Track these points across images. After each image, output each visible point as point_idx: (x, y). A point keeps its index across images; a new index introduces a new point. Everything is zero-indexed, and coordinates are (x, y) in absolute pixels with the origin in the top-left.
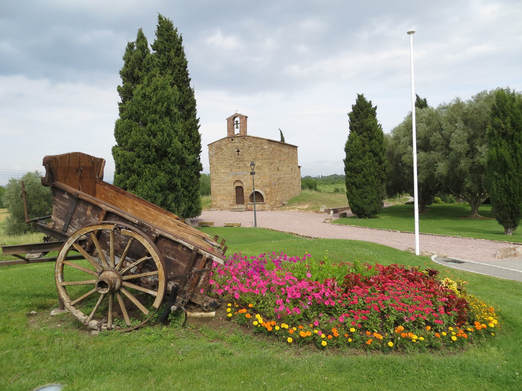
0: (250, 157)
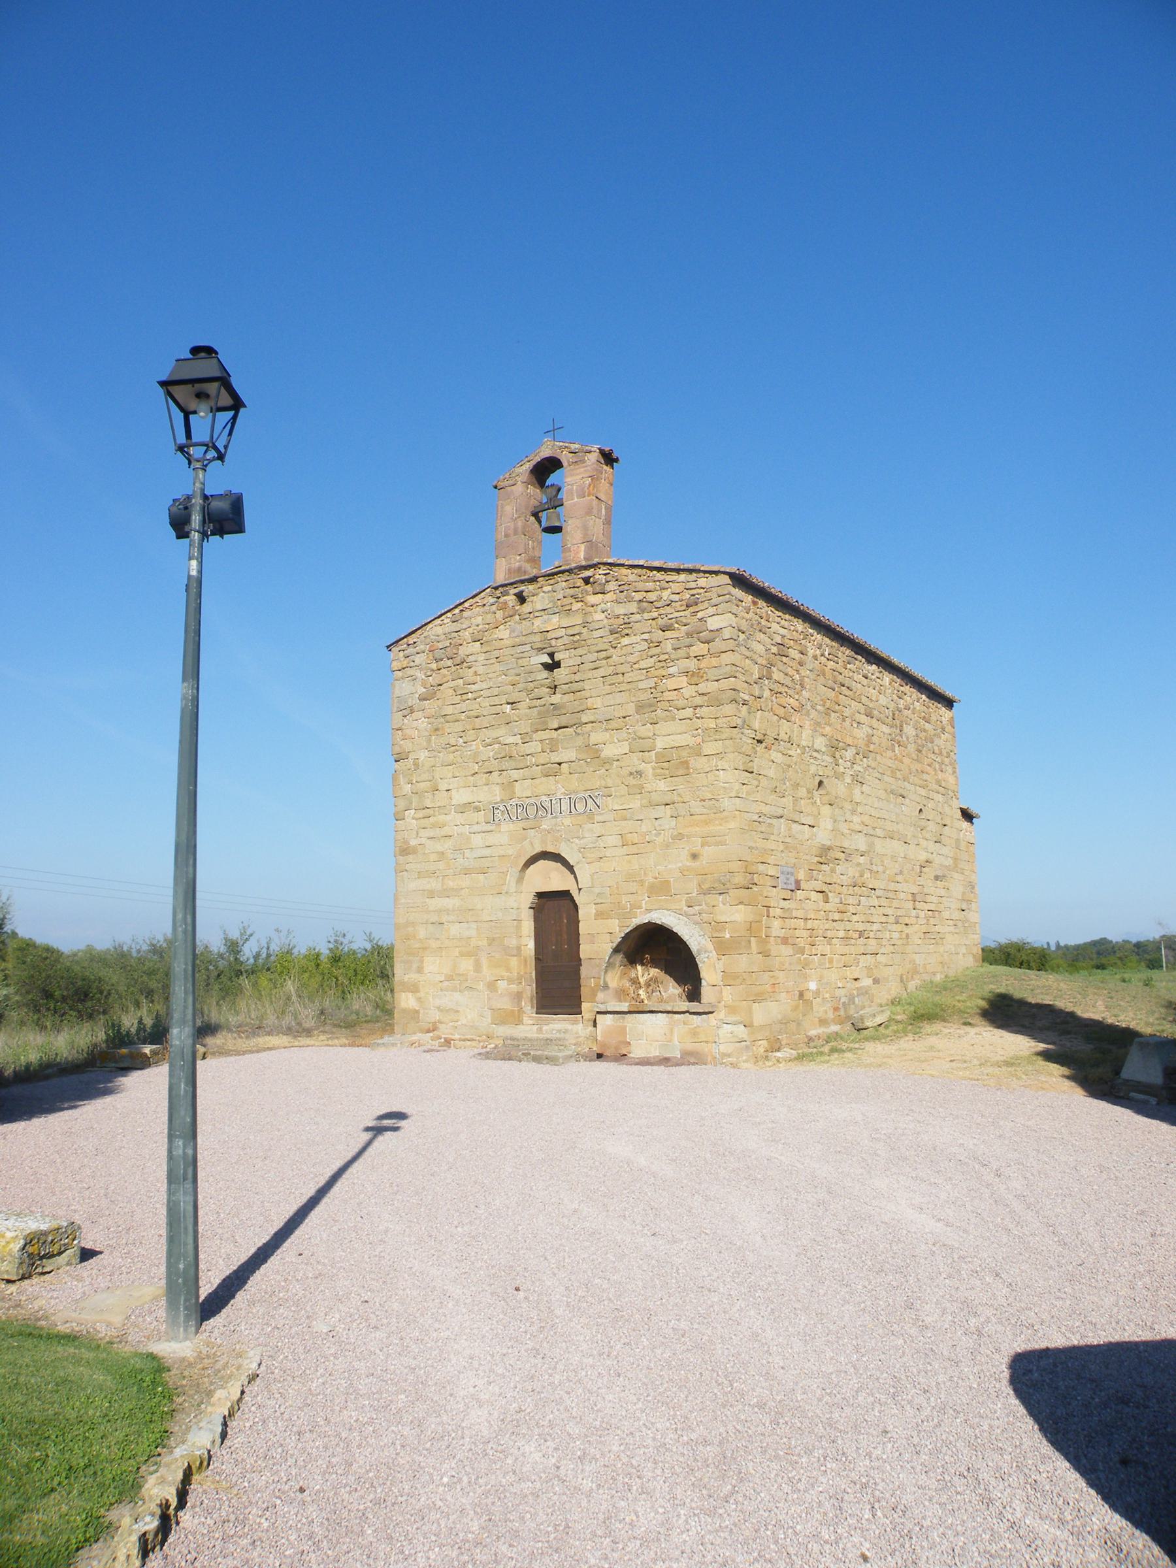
0: (619, 698)
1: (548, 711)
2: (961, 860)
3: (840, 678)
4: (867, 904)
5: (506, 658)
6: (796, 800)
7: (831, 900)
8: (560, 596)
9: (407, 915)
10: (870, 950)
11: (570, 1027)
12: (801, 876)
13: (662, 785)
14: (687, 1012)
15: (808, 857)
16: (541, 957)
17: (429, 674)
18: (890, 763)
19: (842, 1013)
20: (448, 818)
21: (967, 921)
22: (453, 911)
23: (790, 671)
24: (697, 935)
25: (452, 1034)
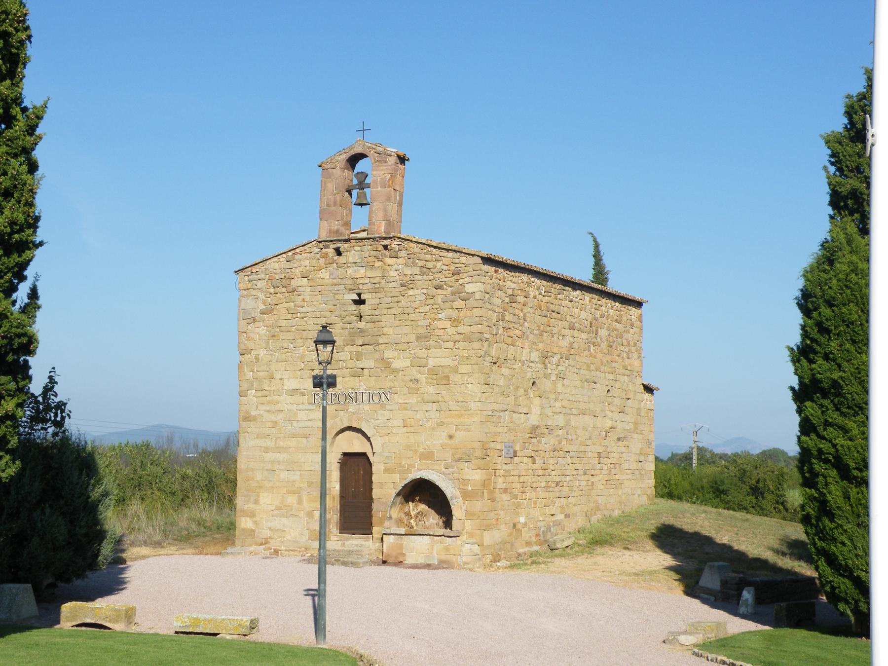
0: (405, 330)
1: (355, 333)
2: (641, 424)
3: (552, 307)
4: (563, 462)
5: (326, 292)
6: (516, 399)
7: (537, 462)
8: (367, 255)
9: (248, 463)
10: (564, 494)
11: (364, 543)
12: (517, 448)
13: (431, 390)
14: (443, 535)
15: (522, 435)
16: (344, 495)
17: (268, 296)
18: (585, 360)
19: (542, 537)
20: (281, 398)
21: (643, 469)
22: (283, 462)
23: (517, 312)
24: (450, 487)
25: (279, 546)
